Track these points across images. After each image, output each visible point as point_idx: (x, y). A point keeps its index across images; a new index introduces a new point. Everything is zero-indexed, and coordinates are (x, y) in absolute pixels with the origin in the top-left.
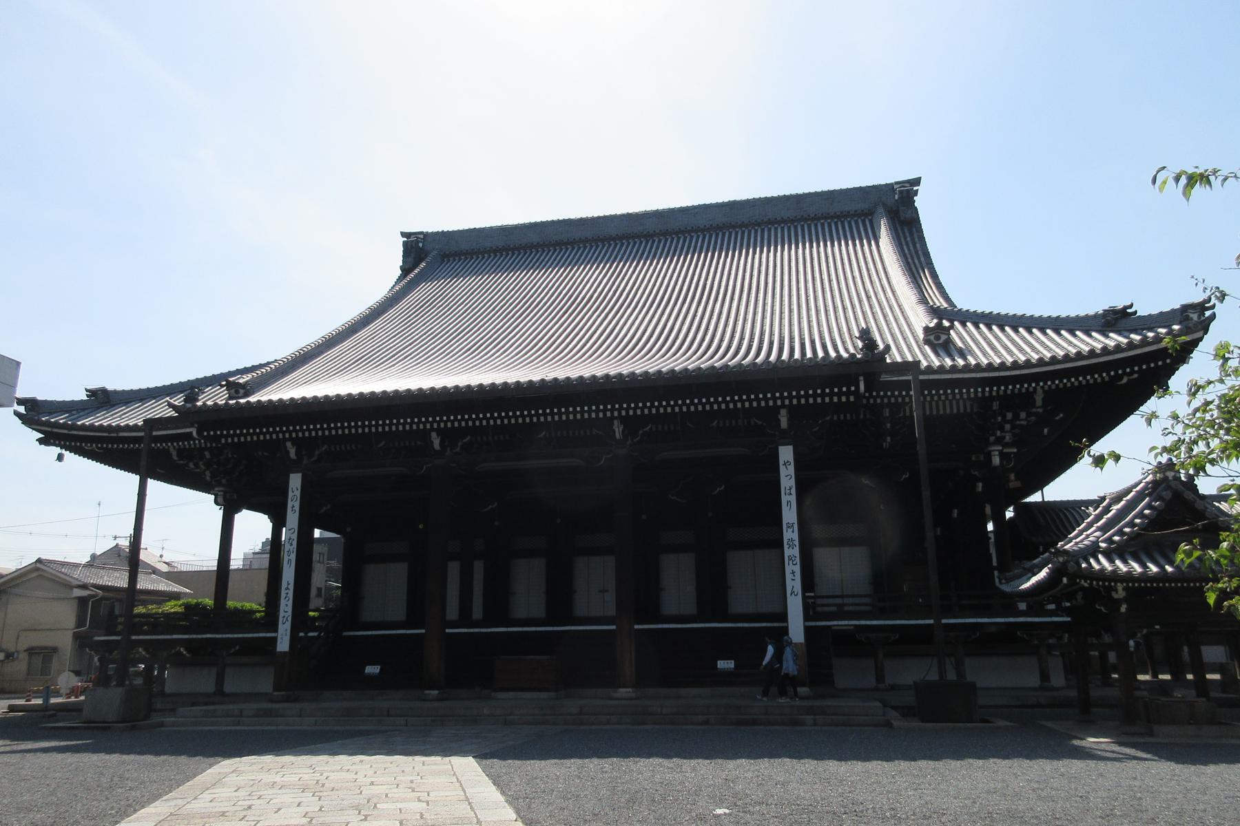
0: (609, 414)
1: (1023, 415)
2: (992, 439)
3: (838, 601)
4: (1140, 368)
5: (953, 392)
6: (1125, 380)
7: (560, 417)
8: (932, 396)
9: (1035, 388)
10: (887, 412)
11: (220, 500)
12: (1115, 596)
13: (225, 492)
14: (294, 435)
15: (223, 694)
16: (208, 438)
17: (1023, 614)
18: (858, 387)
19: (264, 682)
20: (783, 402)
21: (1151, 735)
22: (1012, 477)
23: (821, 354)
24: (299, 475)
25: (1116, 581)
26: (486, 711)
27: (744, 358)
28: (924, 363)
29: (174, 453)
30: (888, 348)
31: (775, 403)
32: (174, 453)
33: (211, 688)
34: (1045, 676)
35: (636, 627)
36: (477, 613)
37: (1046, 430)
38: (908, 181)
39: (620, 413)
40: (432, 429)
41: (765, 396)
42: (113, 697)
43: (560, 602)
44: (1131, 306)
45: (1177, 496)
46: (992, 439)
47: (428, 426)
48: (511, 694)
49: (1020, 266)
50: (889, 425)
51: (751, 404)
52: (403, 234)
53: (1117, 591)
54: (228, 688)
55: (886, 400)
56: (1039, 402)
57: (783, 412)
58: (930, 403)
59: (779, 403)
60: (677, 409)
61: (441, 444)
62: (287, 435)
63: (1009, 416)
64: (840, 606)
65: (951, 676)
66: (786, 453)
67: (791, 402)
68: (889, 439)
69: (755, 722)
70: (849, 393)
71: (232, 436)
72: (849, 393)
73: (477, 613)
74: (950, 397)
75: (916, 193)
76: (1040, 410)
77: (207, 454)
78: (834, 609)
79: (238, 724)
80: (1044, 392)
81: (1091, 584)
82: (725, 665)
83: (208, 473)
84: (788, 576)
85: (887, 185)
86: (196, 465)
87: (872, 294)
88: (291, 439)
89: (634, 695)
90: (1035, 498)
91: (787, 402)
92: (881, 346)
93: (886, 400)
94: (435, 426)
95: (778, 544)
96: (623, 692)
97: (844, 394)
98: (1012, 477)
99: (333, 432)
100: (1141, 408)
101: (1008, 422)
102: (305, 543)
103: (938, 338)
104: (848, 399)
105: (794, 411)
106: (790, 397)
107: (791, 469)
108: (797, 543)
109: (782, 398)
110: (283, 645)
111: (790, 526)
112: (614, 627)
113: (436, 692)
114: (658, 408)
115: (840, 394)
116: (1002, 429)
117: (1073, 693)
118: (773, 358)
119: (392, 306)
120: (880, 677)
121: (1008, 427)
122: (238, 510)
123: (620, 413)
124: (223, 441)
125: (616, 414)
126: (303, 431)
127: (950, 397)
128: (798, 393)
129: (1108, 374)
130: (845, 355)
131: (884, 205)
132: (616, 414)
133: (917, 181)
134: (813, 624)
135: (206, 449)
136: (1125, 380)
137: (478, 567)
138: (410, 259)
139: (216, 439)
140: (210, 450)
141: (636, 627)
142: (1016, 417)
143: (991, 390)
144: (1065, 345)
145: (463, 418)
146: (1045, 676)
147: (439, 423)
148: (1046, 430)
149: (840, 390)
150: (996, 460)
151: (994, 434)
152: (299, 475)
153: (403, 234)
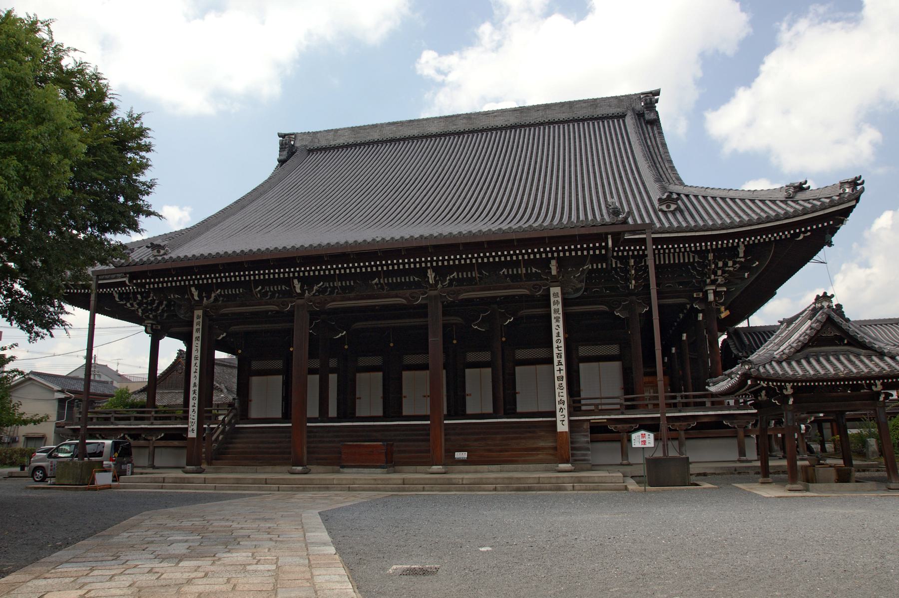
0: (423, 265)
1: (730, 263)
2: (708, 281)
3: (598, 401)
4: (812, 228)
5: (684, 246)
6: (801, 237)
7: (404, 266)
8: (670, 249)
9: (738, 243)
10: (632, 262)
11: (149, 330)
12: (785, 392)
13: (152, 324)
14: (196, 282)
16: (137, 285)
18: (607, 244)
20: (553, 255)
21: (807, 490)
22: (723, 309)
23: (590, 217)
24: (580, 348)
25: (785, 382)
28: (658, 225)
29: (116, 296)
30: (630, 213)
31: (547, 255)
32: (116, 296)
34: (742, 452)
36: (333, 412)
38: (651, 93)
39: (432, 264)
41: (539, 250)
43: (392, 406)
44: (806, 182)
45: (829, 319)
46: (708, 281)
47: (291, 275)
50: (633, 272)
51: (535, 256)
52: (280, 135)
53: (786, 389)
55: (631, 253)
56: (741, 255)
57: (553, 262)
59: (550, 255)
60: (474, 261)
61: (302, 288)
62: (191, 282)
63: (720, 264)
64: (597, 405)
65: (673, 453)
67: (558, 254)
68: (633, 282)
69: (529, 489)
70: (600, 248)
71: (154, 283)
72: (600, 248)
73: (333, 412)
74: (683, 250)
75: (657, 101)
76: (743, 260)
77: (139, 297)
78: (592, 408)
80: (745, 246)
81: (768, 384)
83: (140, 310)
85: (635, 95)
86: (132, 305)
87: (635, 172)
88: (194, 285)
89: (443, 470)
91: (555, 255)
94: (296, 274)
95: (550, 361)
97: (591, 249)
98: (723, 309)
100: (815, 258)
101: (719, 268)
102: (208, 363)
103: (668, 207)
104: (600, 252)
106: (558, 251)
109: (552, 252)
112: (429, 422)
113: (300, 468)
114: (459, 260)
115: (594, 248)
116: (715, 274)
117: (758, 464)
118: (556, 222)
119: (271, 188)
121: (719, 272)
122: (162, 338)
123: (432, 264)
124: (147, 287)
125: (429, 264)
126: (541, 253)
127: (683, 250)
128: (576, 247)
129: (789, 232)
131: (633, 110)
132: (296, 274)
133: (657, 93)
135: (138, 293)
136: (801, 237)
137: (333, 378)
138: (285, 153)
139: (143, 285)
140: (141, 293)
142: (725, 265)
143: (717, 244)
144: (758, 211)
145: (497, 255)
146: (742, 452)
149: (594, 245)
150: (711, 297)
151: (710, 277)
152: (580, 348)
153: (280, 135)
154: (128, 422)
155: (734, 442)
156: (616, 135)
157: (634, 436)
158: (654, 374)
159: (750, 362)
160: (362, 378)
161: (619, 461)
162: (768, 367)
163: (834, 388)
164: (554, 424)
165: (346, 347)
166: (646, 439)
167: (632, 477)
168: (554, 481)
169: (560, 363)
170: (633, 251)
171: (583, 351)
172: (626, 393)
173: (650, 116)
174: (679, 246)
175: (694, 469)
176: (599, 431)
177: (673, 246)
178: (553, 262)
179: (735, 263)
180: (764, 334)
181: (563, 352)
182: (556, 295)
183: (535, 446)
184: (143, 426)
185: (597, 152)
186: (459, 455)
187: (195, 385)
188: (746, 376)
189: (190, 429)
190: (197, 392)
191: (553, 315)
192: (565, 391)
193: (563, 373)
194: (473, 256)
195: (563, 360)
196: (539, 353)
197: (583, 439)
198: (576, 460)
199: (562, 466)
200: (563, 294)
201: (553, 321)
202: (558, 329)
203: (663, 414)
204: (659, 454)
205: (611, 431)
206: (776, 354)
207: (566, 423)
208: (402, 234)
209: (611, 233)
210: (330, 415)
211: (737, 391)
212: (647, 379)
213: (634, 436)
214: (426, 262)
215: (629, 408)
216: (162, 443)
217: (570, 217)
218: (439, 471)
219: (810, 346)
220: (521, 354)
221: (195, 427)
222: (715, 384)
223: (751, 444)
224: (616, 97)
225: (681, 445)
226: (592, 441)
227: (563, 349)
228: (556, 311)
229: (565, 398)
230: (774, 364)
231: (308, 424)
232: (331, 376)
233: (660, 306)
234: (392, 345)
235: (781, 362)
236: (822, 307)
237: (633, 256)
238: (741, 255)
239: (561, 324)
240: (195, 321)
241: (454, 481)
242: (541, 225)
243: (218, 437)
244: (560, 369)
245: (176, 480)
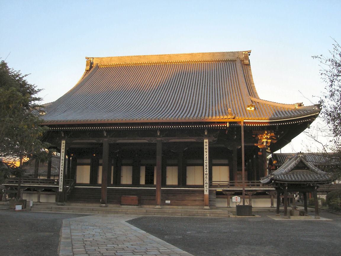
2: (264, 137)
15: (40, 202)
17: (143, 186)
18: (227, 126)
19: (52, 199)
26: (120, 211)
33: (36, 200)
34: (272, 204)
35: (162, 188)
37: (279, 136)
46: (264, 137)
48: (126, 206)
49: (277, 87)
54: (41, 201)
56: (277, 129)
65: (246, 204)
68: (235, 137)
75: (249, 55)
79: (51, 211)
89: (161, 207)
90: (278, 152)
95: (202, 165)
96: (157, 207)
110: (61, 190)
113: (104, 205)
134: (202, 189)
138: (89, 67)
141: (162, 188)
148: (279, 136)
154: (29, 183)
155: (269, 200)
157: (233, 198)
158: (241, 170)
159: (273, 175)
161: (226, 206)
162: (280, 176)
163: (300, 185)
164: (203, 191)
166: (237, 199)
167: (231, 212)
168: (203, 213)
169: (206, 169)
172: (230, 180)
173: (246, 62)
175: (253, 210)
176: (219, 194)
180: (284, 157)
181: (208, 164)
182: (206, 143)
183: (195, 199)
184: (35, 185)
185: (196, 75)
186: (167, 202)
187: (62, 171)
188: (272, 179)
189: (60, 188)
190: (63, 173)
191: (205, 150)
192: (208, 179)
193: (208, 172)
195: (208, 168)
196: (199, 162)
197: (214, 197)
198: (211, 205)
199: (206, 207)
200: (209, 142)
201: (205, 152)
203: (244, 189)
204: (242, 204)
205: (224, 194)
206: (283, 172)
207: (208, 191)
211: (269, 184)
212: (238, 172)
213: (233, 198)
215: (231, 186)
216: (43, 192)
218: (159, 208)
219: (294, 170)
221: (62, 187)
222: (263, 179)
223: (275, 200)
224: (232, 52)
225: (250, 201)
226: (217, 198)
227: (208, 163)
228: (206, 149)
229: (208, 182)
230: (282, 175)
231: (108, 187)
232: (156, 184)
233: (245, 147)
235: (284, 175)
236: (299, 156)
239: (208, 154)
240: (62, 145)
243: (69, 191)
244: (206, 171)
245: (56, 208)
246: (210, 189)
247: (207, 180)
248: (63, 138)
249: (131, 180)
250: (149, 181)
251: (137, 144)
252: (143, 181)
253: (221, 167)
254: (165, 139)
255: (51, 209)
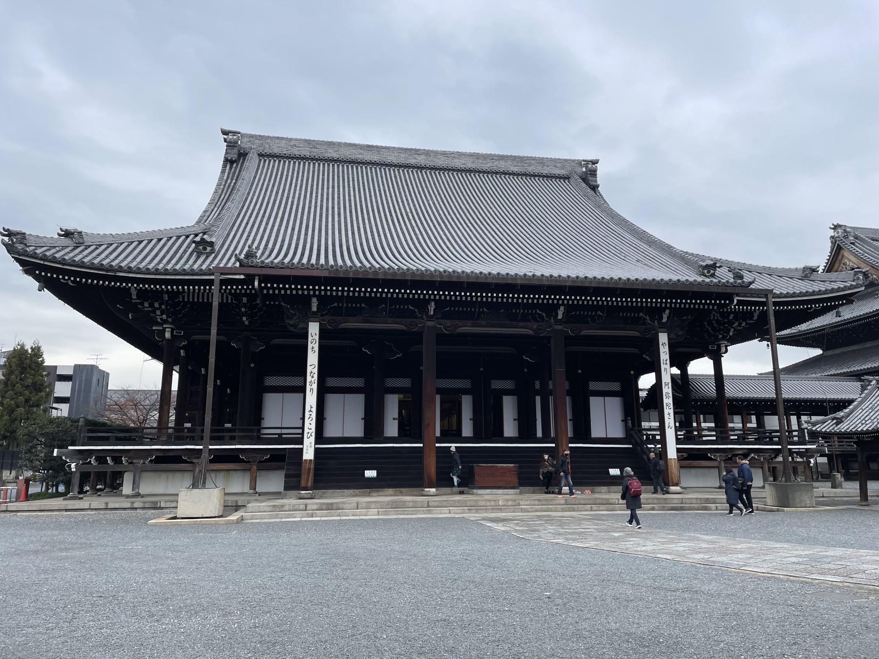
1: (744, 324)
3: (279, 431)
7: (487, 299)
10: (245, 300)
20: (314, 293)
27: (275, 258)
36: (467, 430)
40: (563, 304)
42: (251, 491)
48: (488, 491)
54: (143, 490)
56: (755, 318)
57: (562, 308)
58: (203, 294)
59: (312, 293)
64: (280, 435)
66: (663, 338)
67: (320, 293)
77: (166, 297)
82: (371, 474)
84: (666, 416)
88: (435, 300)
92: (396, 267)
93: (243, 291)
95: (302, 390)
99: (289, 292)
105: (569, 308)
107: (667, 347)
108: (671, 395)
110: (309, 454)
111: (667, 384)
113: (433, 490)
118: (296, 261)
120: (253, 487)
125: (668, 305)
126: (286, 289)
130: (358, 264)
142: (740, 325)
147: (568, 300)
153: (836, 227)
156: (380, 191)
160: (596, 404)
165: (482, 369)
170: (563, 300)
171: (331, 382)
174: (455, 293)
177: (471, 294)
178: (562, 308)
179: (747, 324)
185: (361, 206)
194: (400, 291)
196: (295, 381)
202: (313, 359)
208: (680, 278)
209: (259, 276)
210: (464, 435)
214: (666, 303)
217: (293, 258)
220: (270, 381)
234: (482, 369)
237: (245, 295)
238: (755, 318)
241: (611, 501)
242: (272, 262)
244: (311, 399)
246: (317, 446)
247: (310, 425)
248: (314, 317)
249: (362, 423)
250: (411, 427)
251: (494, 326)
252: (392, 428)
253: (286, 395)
254: (445, 326)
255: (428, 506)
